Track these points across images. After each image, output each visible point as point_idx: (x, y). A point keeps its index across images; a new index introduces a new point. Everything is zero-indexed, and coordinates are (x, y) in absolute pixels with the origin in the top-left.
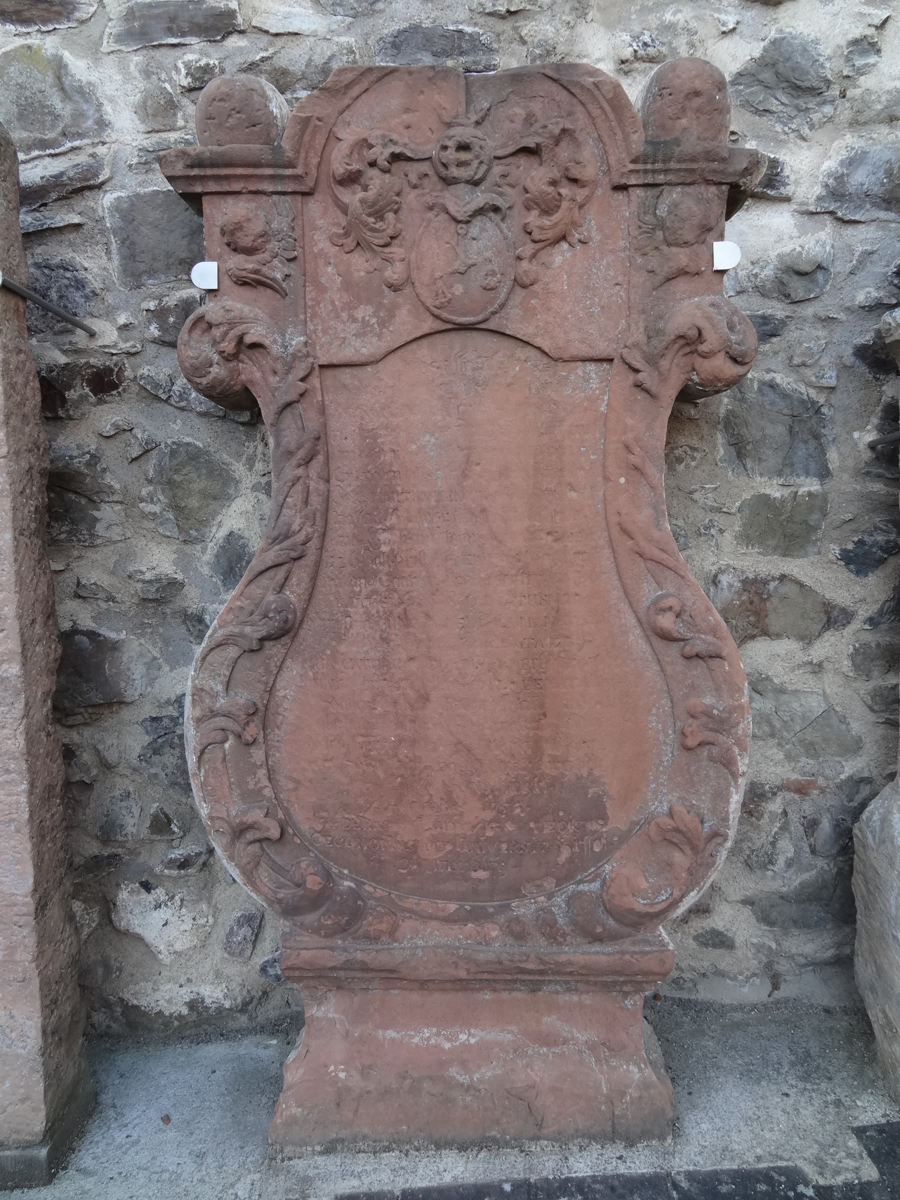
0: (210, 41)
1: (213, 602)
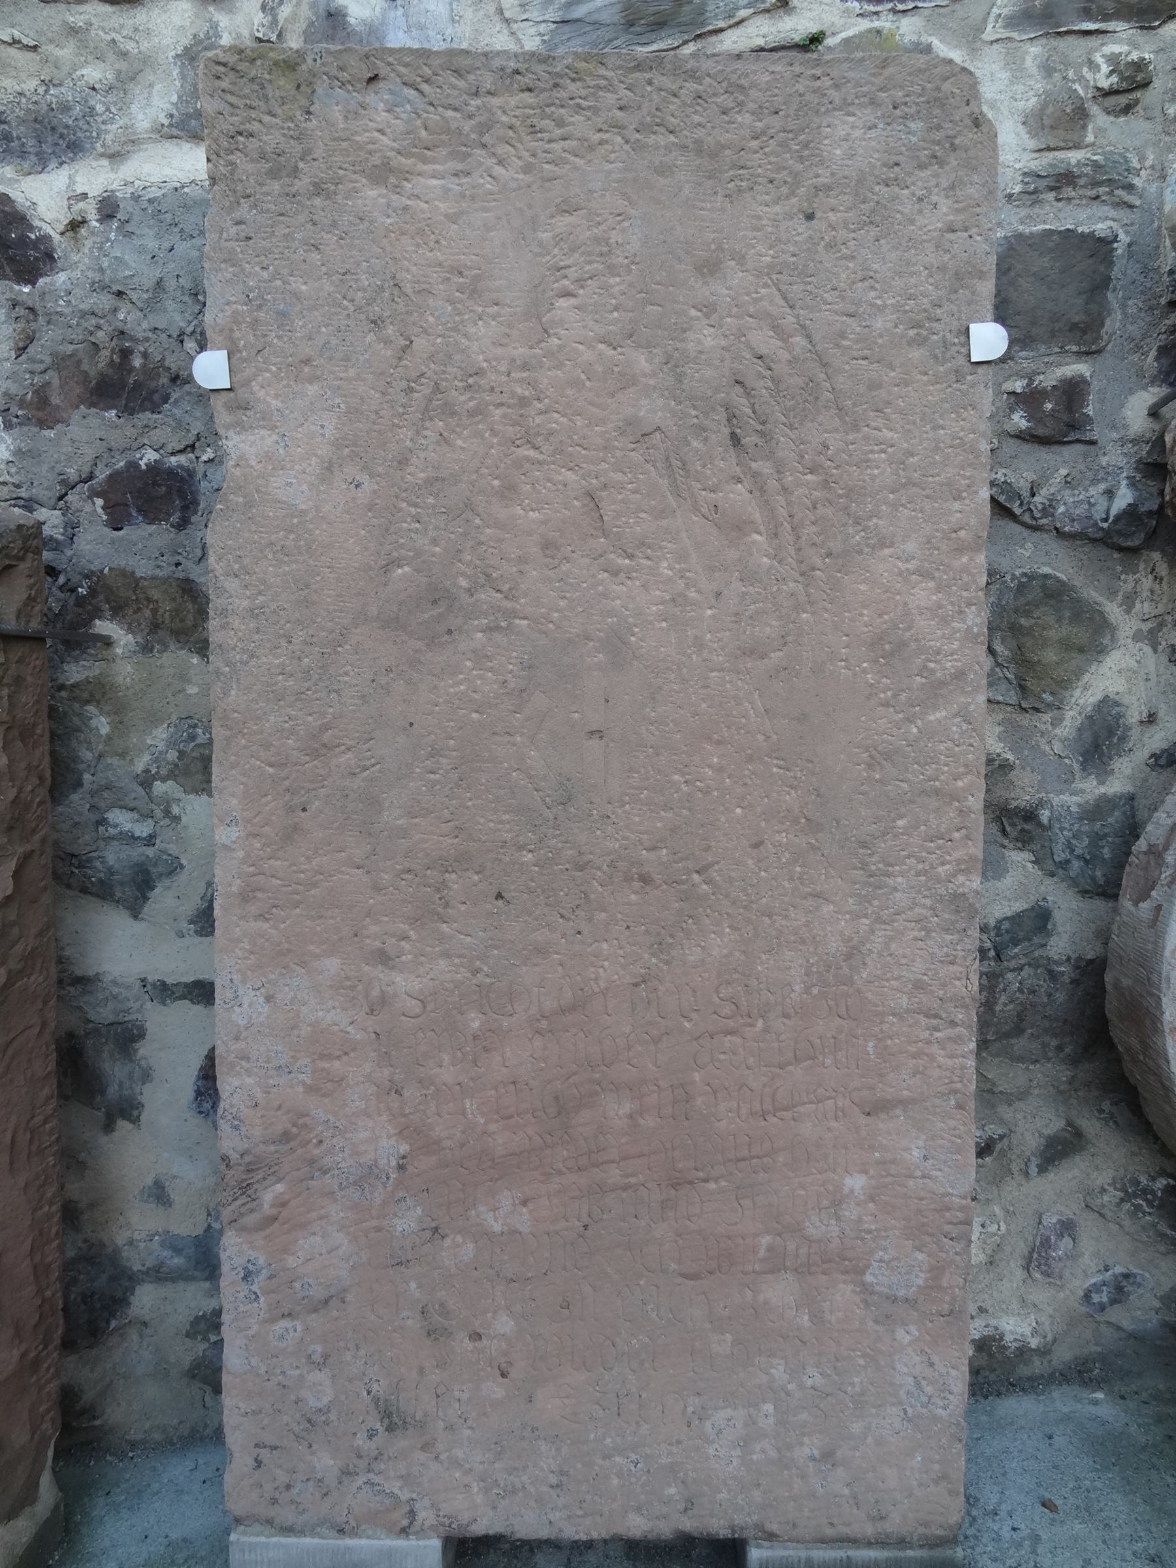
0: (1141, 28)
1: (1062, 792)
